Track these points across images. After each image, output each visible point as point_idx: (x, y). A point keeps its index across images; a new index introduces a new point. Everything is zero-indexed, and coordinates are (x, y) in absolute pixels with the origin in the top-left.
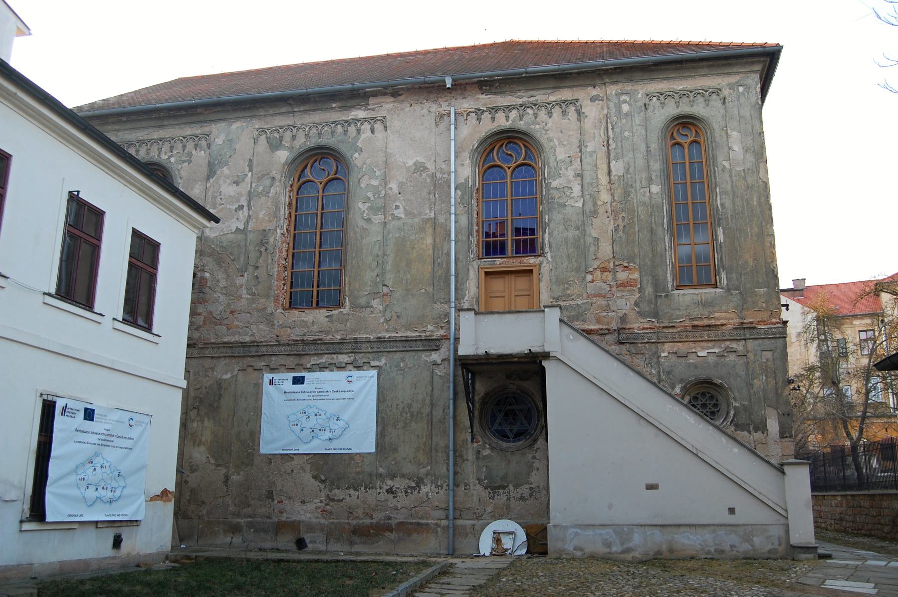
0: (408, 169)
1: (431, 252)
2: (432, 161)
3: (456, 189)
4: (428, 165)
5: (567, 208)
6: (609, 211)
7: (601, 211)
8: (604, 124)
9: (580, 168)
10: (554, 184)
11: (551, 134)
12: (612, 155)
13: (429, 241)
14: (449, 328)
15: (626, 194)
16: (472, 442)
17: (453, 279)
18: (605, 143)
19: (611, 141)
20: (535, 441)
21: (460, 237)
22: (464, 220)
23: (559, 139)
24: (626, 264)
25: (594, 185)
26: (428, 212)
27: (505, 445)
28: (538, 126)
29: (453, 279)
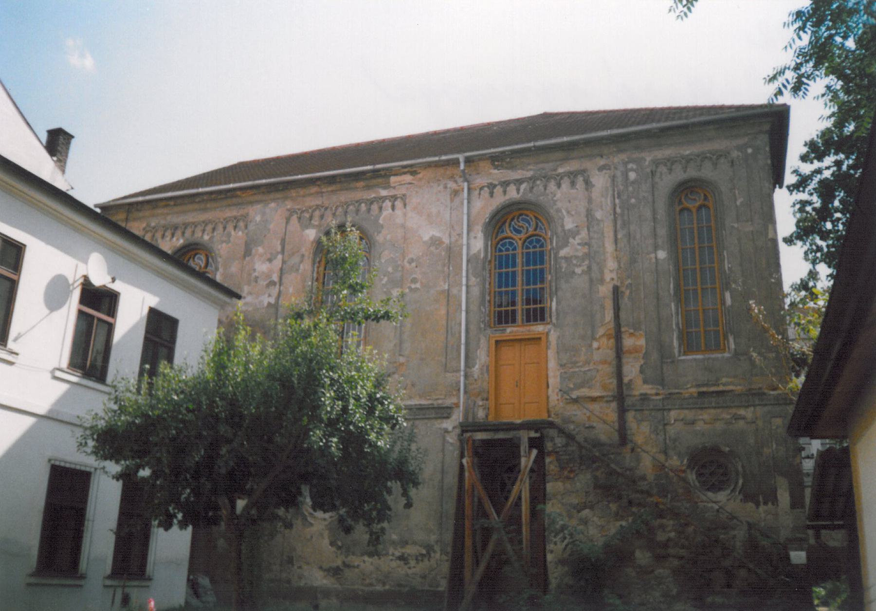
9: (587, 237)
10: (563, 253)
26: (442, 283)
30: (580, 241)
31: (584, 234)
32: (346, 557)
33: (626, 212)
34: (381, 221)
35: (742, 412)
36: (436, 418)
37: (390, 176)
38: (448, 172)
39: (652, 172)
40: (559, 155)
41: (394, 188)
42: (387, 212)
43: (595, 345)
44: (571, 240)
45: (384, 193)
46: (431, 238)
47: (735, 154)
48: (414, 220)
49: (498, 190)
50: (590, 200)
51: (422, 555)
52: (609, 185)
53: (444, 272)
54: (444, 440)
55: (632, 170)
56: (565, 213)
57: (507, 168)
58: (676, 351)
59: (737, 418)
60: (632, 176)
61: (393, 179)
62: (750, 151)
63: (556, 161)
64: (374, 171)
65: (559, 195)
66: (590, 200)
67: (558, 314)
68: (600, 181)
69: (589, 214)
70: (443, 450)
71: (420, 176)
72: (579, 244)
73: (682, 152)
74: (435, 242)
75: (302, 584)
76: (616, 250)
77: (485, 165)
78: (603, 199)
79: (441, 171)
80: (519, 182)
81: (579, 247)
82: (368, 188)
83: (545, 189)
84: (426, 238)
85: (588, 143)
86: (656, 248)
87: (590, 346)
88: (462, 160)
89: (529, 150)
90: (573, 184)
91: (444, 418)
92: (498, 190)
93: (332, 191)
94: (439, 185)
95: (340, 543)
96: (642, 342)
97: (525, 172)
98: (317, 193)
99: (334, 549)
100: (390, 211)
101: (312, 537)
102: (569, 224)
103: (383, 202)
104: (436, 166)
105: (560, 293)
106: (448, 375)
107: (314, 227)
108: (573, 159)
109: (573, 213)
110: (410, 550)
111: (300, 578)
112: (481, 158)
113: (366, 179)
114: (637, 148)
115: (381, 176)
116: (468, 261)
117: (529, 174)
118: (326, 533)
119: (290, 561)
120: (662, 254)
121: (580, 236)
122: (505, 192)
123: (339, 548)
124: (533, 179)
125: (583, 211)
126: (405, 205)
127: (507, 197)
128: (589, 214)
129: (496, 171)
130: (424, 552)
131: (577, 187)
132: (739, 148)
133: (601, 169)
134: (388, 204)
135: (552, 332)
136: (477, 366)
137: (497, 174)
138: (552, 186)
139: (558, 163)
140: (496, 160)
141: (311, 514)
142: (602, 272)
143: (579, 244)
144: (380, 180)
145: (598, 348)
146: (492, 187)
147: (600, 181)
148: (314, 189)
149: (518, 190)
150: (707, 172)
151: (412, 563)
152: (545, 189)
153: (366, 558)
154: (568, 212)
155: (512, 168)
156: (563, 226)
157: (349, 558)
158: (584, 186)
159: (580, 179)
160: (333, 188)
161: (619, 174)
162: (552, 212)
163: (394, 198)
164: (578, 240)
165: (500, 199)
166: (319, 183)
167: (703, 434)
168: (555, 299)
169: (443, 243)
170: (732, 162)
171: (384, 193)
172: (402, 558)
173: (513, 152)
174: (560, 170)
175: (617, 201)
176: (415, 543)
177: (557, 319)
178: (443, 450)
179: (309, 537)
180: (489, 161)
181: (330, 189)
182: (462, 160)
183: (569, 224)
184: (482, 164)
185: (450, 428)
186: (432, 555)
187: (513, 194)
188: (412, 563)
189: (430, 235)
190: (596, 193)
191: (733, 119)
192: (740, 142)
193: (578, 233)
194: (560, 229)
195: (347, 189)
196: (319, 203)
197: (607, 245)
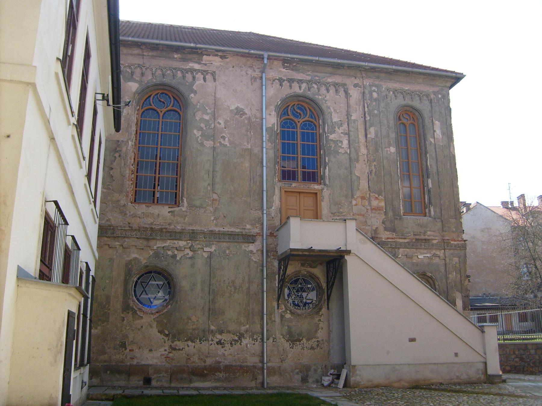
0: (231, 111)
1: (248, 172)
4: (246, 111)
6: (366, 160)
7: (361, 159)
8: (362, 103)
9: (347, 129)
10: (332, 137)
12: (368, 124)
14: (263, 228)
15: (376, 150)
16: (278, 308)
17: (265, 193)
19: (367, 115)
20: (321, 309)
23: (334, 108)
24: (377, 196)
26: (246, 144)
27: (299, 312)
28: (320, 97)
30: (342, 131)
31: (345, 126)
32: (173, 342)
33: (372, 117)
34: (194, 87)
35: (438, 253)
36: (243, 242)
37: (204, 55)
38: (249, 63)
39: (386, 95)
40: (330, 70)
41: (206, 65)
42: (200, 81)
43: (354, 202)
44: (337, 129)
45: (197, 66)
46: (237, 108)
47: (432, 96)
48: (221, 93)
49: (286, 84)
50: (348, 106)
51: (235, 340)
52: (360, 98)
53: (247, 135)
54: (250, 260)
55: (374, 91)
56: (332, 110)
57: (292, 70)
58: (402, 212)
59: (435, 255)
60: (375, 95)
61: (205, 57)
62: (440, 96)
63: (326, 73)
64: (249, 53)
65: (328, 97)
66: (348, 106)
67: (329, 179)
68: (355, 94)
69: (348, 115)
70: (249, 266)
71: (227, 60)
72: (342, 133)
73: (403, 87)
74: (239, 112)
75: (135, 362)
76: (366, 141)
77: (277, 64)
78: (357, 107)
79: (244, 60)
80: (300, 82)
81: (342, 135)
82: (184, 60)
83: (319, 91)
84: (233, 108)
85: (350, 67)
86: (390, 145)
87: (351, 202)
88: (266, 56)
89: (311, 61)
90: (337, 91)
91: (251, 243)
92: (286, 84)
93: (153, 56)
94: (241, 71)
95: (167, 332)
96: (383, 204)
97: (305, 76)
98: (139, 55)
99: (162, 336)
100: (202, 81)
101: (142, 327)
102: (335, 119)
103: (197, 74)
104: (242, 56)
105: (330, 164)
106: (252, 212)
107: (135, 81)
108: (338, 74)
109: (338, 111)
110: (225, 337)
111: (132, 358)
112: (277, 58)
113: (184, 53)
114: (378, 78)
115: (197, 53)
116: (266, 129)
117: (309, 78)
118: (155, 324)
119: (123, 345)
120: (393, 150)
121: (343, 128)
122: (291, 86)
123: (167, 335)
124: (308, 82)
125: (345, 113)
126: (215, 80)
127: (292, 91)
128: (348, 115)
129: (284, 70)
130: (236, 338)
132: (435, 93)
133: (356, 86)
134: (200, 76)
135: (325, 190)
136: (273, 208)
137: (285, 73)
138: (323, 90)
139: (328, 75)
140: (285, 62)
141: (140, 309)
142: (357, 155)
143: (342, 133)
144: (194, 56)
145: (356, 205)
146: (281, 81)
147: (355, 94)
148: (136, 51)
149: (300, 88)
150: (416, 103)
151: (228, 346)
152: (319, 91)
153: (190, 343)
154: (335, 110)
155: (297, 70)
156: (331, 118)
157: (175, 343)
158: (344, 94)
159: (342, 90)
160: (154, 53)
161: (367, 92)
162: (324, 107)
163: (204, 73)
164: (341, 130)
165: (286, 91)
166: (143, 47)
167: (417, 265)
168: (327, 167)
169: (244, 114)
170: (431, 100)
171: (197, 66)
172: (219, 343)
173: (302, 60)
174: (329, 80)
175: (366, 109)
176: (229, 332)
177: (329, 182)
178: (249, 266)
179: (139, 327)
180: (281, 62)
181: (150, 54)
182: (266, 56)
183: (335, 119)
184: (276, 62)
185: (255, 251)
186: (243, 340)
187: (296, 89)
188: (228, 346)
190: (352, 101)
191: (434, 76)
192: (436, 89)
193: (341, 125)
194: (329, 121)
195: (165, 57)
196: (141, 63)
197: (360, 137)
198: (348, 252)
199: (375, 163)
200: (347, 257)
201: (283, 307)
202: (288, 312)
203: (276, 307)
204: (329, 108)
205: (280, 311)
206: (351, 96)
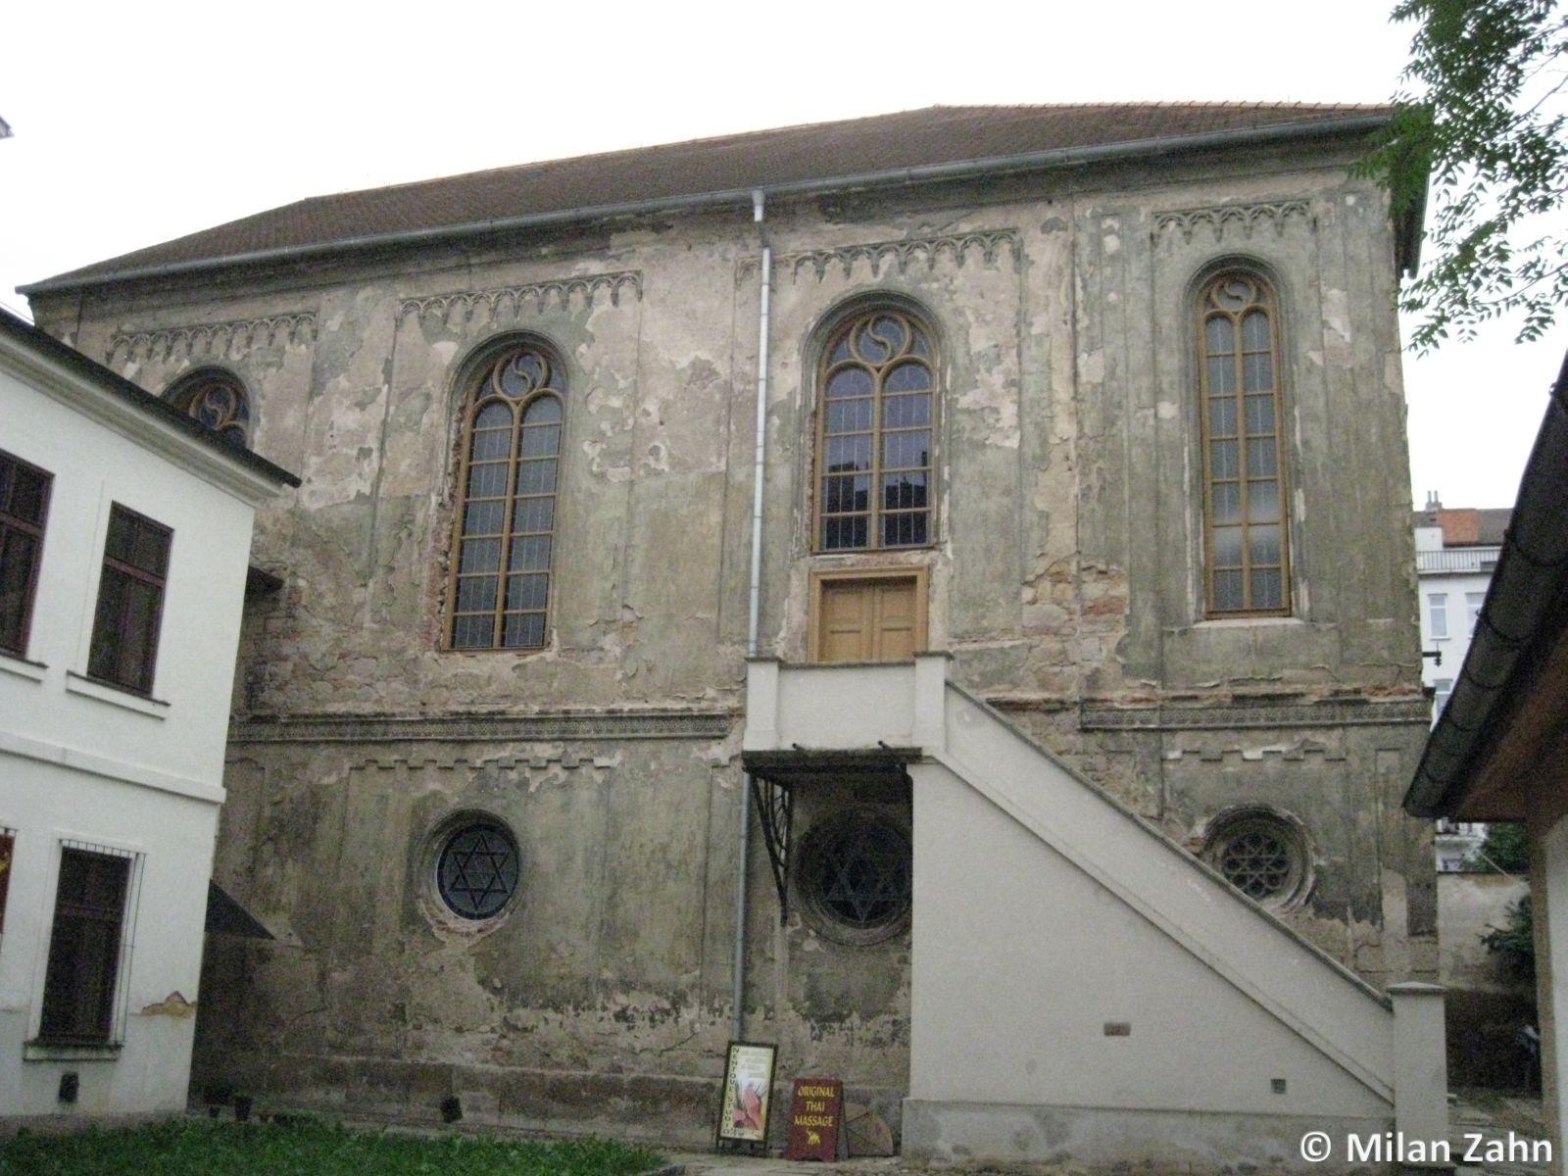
1: (716, 540)
2: (726, 357)
3: (769, 414)
5: (989, 451)
11: (960, 300)
13: (715, 518)
18: (1069, 317)
21: (774, 510)
22: (783, 476)
24: (1102, 567)
25: (1044, 403)
26: (714, 459)
29: (754, 594)
131: (999, 264)
168: (946, 497)
189: (692, 356)
198: (915, 756)
199: (1100, 464)
200: (912, 771)
201: (798, 918)
202: (812, 933)
203: (778, 916)
204: (962, 313)
205: (789, 930)
206: (1033, 263)
